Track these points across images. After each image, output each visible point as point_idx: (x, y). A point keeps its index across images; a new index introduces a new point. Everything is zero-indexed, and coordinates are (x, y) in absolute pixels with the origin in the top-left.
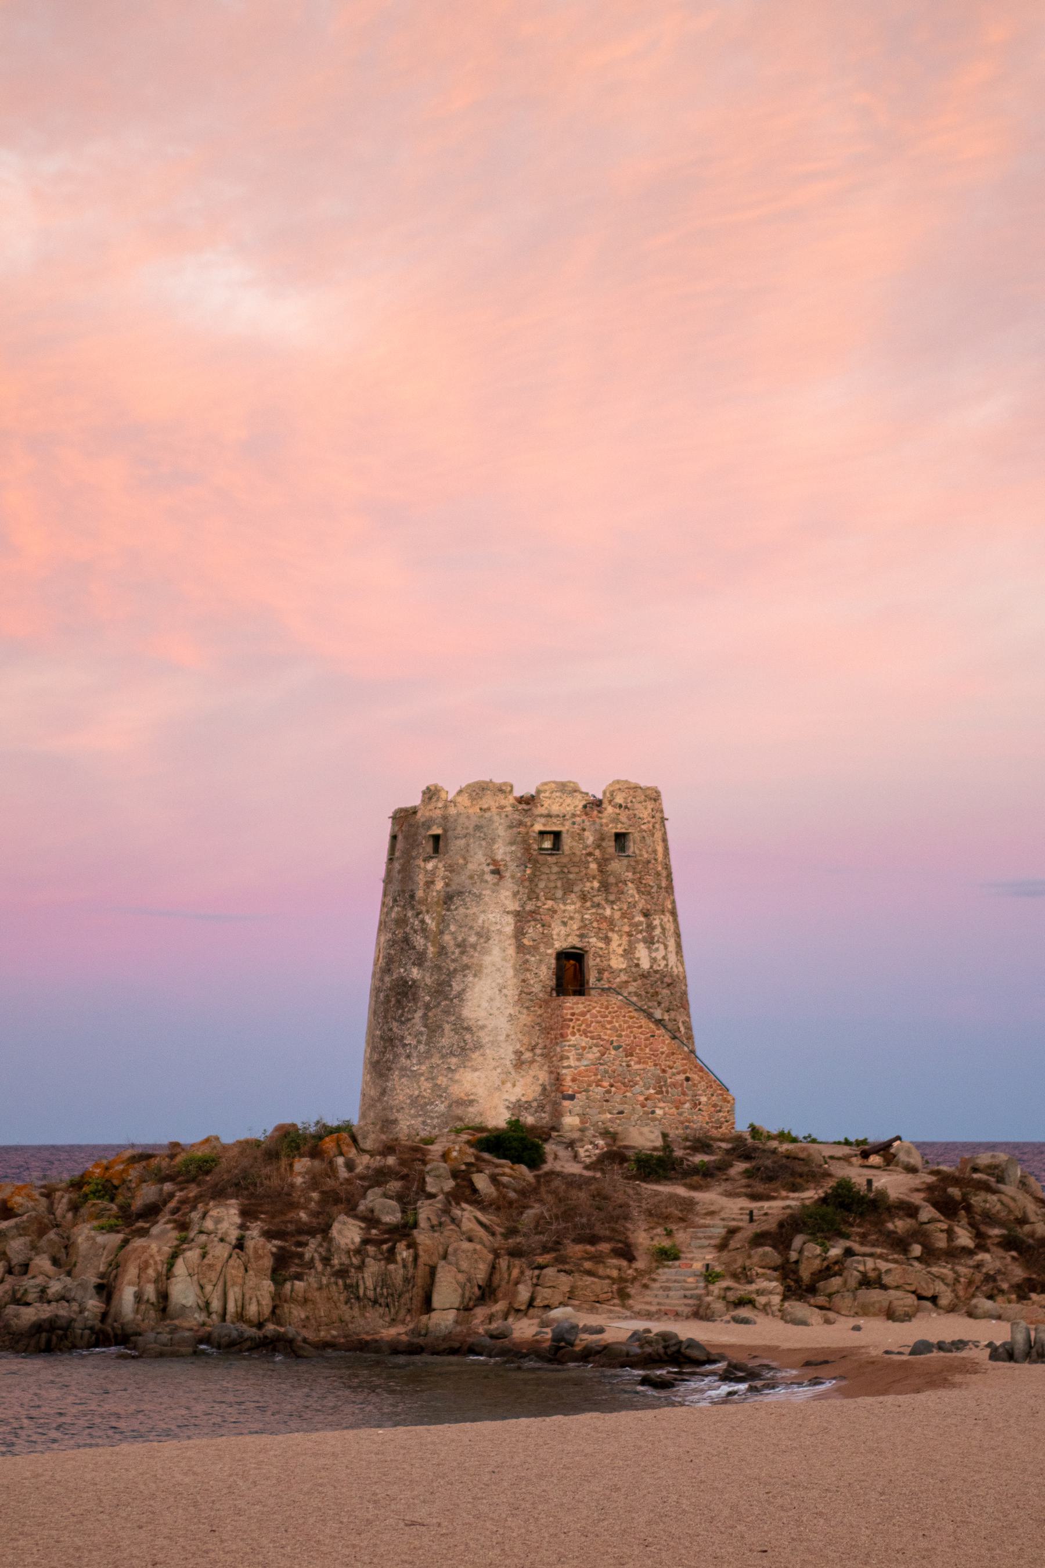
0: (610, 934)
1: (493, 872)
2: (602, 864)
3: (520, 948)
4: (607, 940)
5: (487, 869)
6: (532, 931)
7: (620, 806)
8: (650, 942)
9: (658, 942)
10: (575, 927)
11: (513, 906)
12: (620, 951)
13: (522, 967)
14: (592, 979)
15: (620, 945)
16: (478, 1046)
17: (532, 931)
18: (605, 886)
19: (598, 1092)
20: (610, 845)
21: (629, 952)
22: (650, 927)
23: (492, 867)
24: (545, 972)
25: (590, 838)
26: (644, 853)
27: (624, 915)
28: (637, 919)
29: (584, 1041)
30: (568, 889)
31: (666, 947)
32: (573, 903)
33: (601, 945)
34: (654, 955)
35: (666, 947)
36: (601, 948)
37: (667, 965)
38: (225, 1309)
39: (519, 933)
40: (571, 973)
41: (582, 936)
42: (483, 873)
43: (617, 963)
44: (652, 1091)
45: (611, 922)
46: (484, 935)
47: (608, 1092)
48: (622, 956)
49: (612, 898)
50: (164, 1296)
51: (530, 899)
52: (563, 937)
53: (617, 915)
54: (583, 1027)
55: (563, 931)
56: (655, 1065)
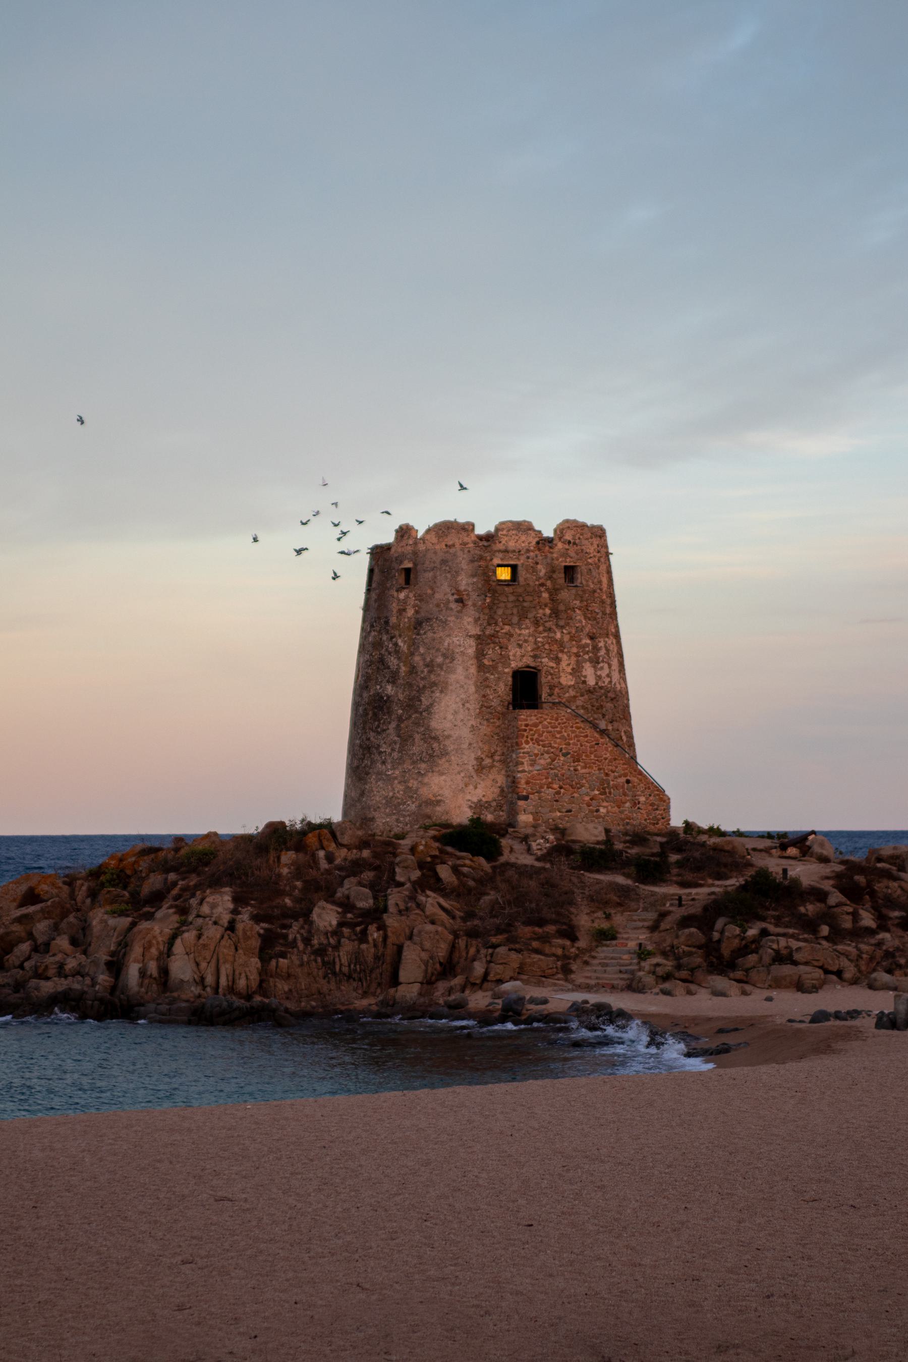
0: (560, 655)
1: (457, 601)
2: (554, 592)
3: (481, 667)
4: (558, 660)
5: (452, 598)
6: (491, 652)
7: (569, 542)
8: (595, 662)
9: (603, 661)
10: (529, 649)
11: (475, 630)
12: (569, 670)
13: (483, 685)
14: (544, 694)
15: (569, 665)
16: (445, 753)
17: (491, 652)
18: (556, 613)
19: (548, 793)
20: (560, 576)
21: (577, 671)
22: (596, 649)
23: (456, 597)
24: (503, 688)
25: (542, 570)
26: (590, 583)
27: (572, 639)
28: (584, 641)
29: (537, 749)
30: (523, 616)
31: (610, 666)
32: (527, 628)
33: (552, 664)
34: (599, 673)
35: (610, 666)
36: (552, 668)
37: (610, 682)
38: (218, 983)
39: (480, 655)
40: (526, 689)
41: (535, 657)
42: (448, 601)
43: (567, 680)
44: (597, 792)
45: (561, 645)
46: (449, 656)
47: (558, 793)
48: (571, 674)
49: (561, 623)
50: (164, 971)
51: (490, 625)
52: (519, 657)
53: (566, 638)
54: (536, 736)
55: (519, 652)
56: (600, 769)
